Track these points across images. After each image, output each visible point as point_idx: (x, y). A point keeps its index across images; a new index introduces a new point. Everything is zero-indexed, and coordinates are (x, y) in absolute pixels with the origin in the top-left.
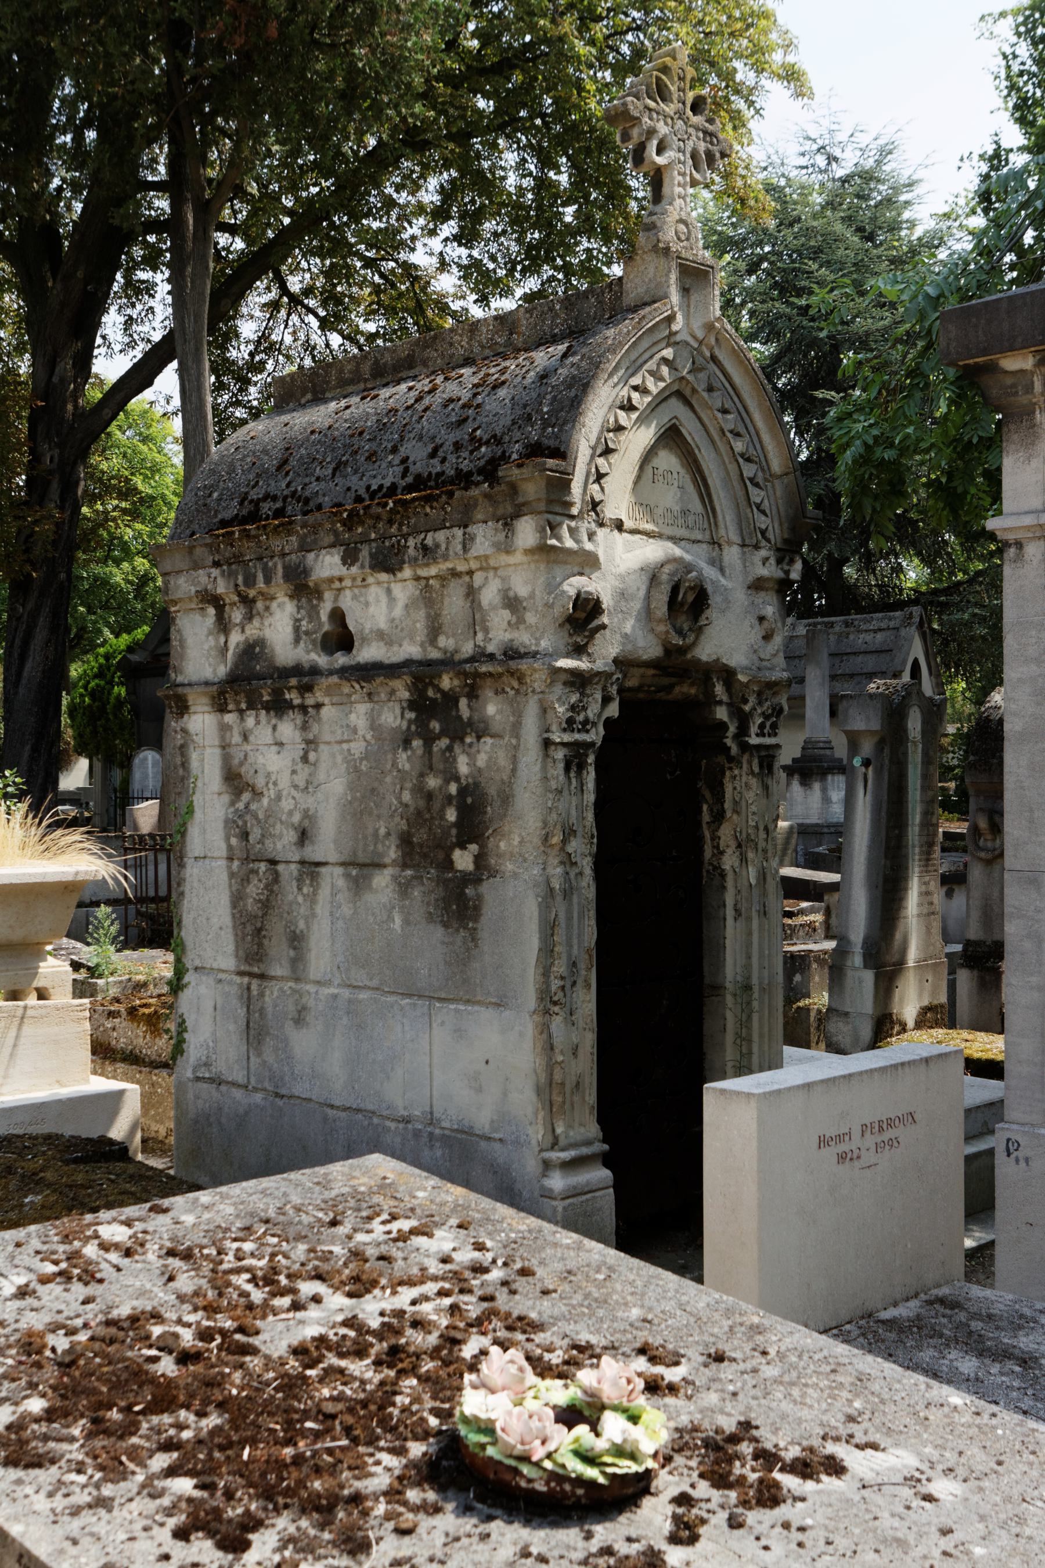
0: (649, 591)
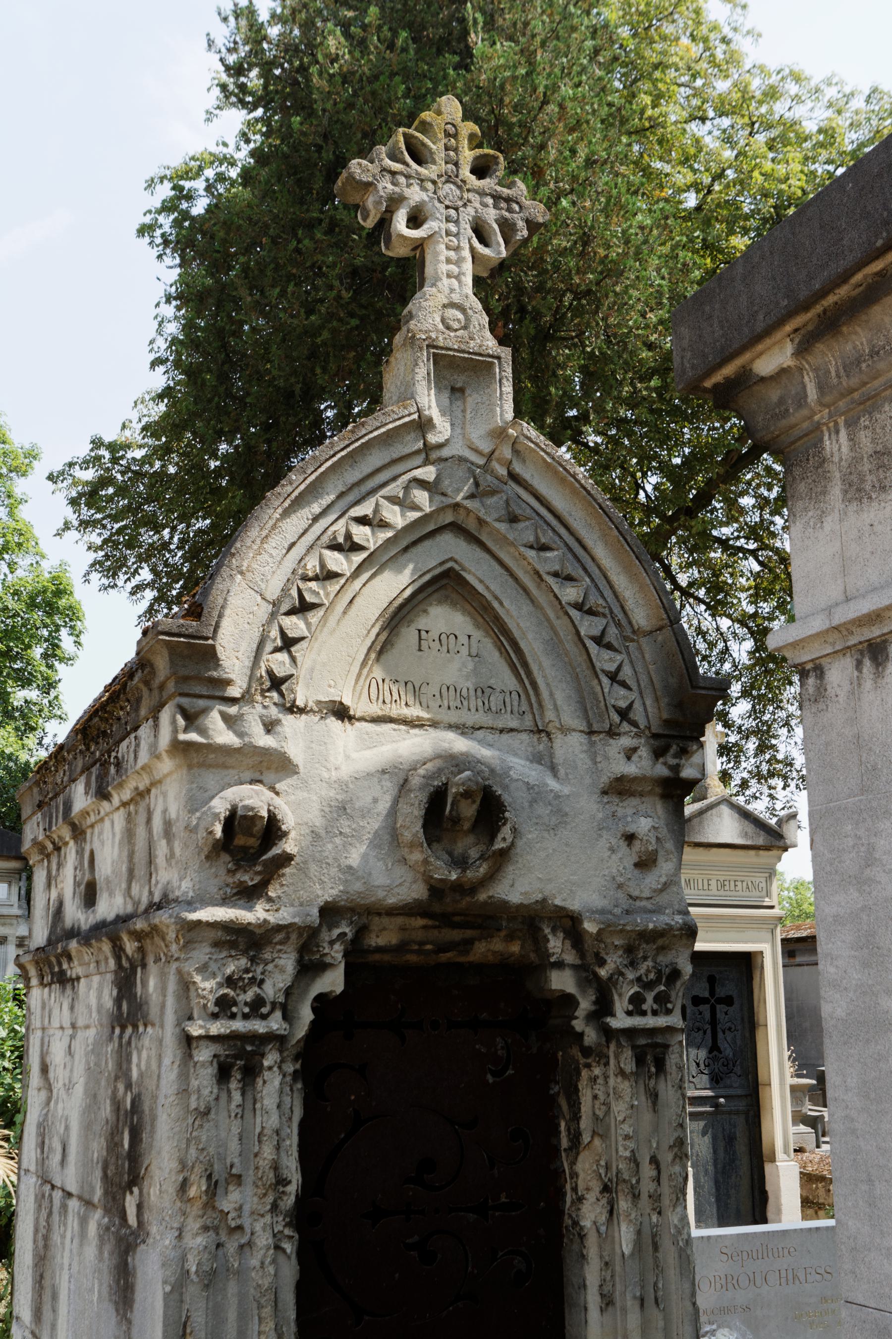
0: (396, 802)
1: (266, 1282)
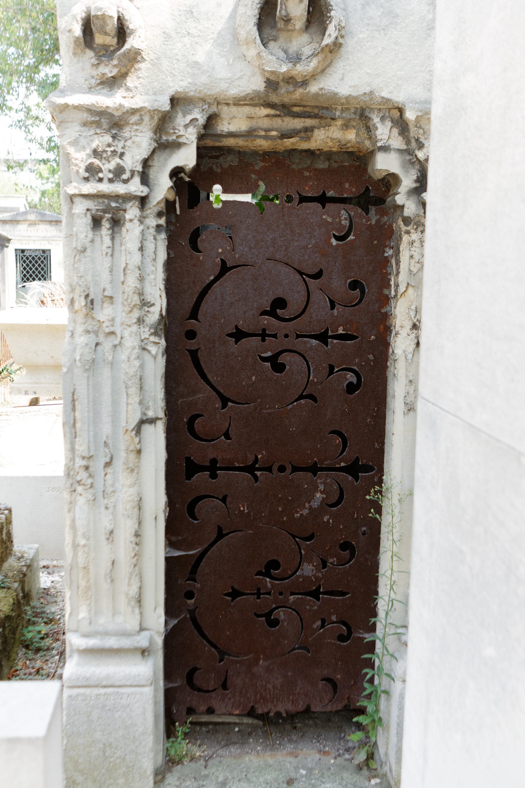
1: (132, 371)
